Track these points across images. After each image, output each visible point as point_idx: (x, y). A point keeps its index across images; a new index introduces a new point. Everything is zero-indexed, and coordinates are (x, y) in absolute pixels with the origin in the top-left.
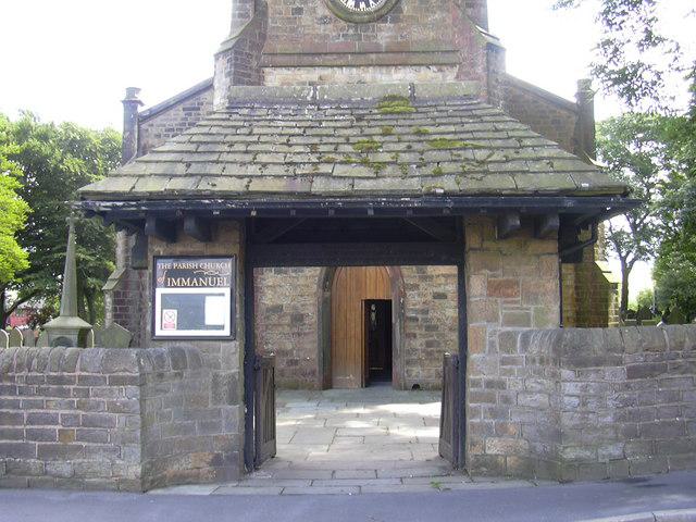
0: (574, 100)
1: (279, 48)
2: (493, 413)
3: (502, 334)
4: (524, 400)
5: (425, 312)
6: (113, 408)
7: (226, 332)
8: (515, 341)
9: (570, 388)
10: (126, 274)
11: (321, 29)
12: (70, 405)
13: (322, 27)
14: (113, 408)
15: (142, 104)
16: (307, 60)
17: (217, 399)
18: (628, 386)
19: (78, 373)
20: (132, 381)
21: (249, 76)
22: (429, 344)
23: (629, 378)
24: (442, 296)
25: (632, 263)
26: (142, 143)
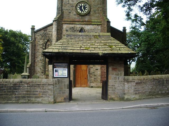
0: (122, 31)
1: (66, 20)
2: (112, 90)
3: (115, 77)
4: (118, 88)
5: (94, 73)
6: (49, 89)
7: (67, 76)
8: (117, 78)
9: (126, 86)
10: (31, 64)
11: (74, 16)
12: (40, 89)
13: (75, 16)
14: (49, 89)
15: (35, 29)
16: (71, 23)
17: (65, 88)
18: (136, 86)
19: (42, 83)
20: (52, 85)
21: (60, 25)
22: (95, 79)
23: (136, 84)
24: (97, 69)
25: (131, 62)
26: (35, 37)
